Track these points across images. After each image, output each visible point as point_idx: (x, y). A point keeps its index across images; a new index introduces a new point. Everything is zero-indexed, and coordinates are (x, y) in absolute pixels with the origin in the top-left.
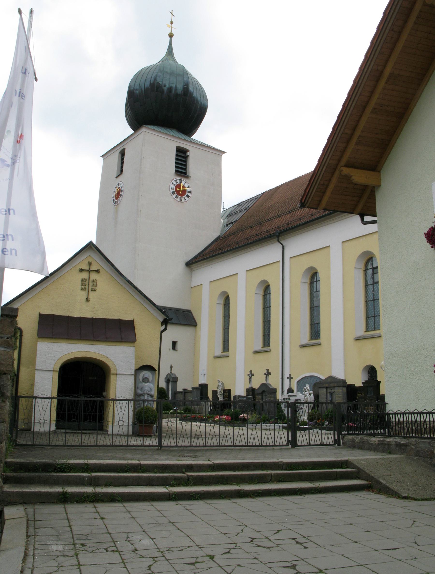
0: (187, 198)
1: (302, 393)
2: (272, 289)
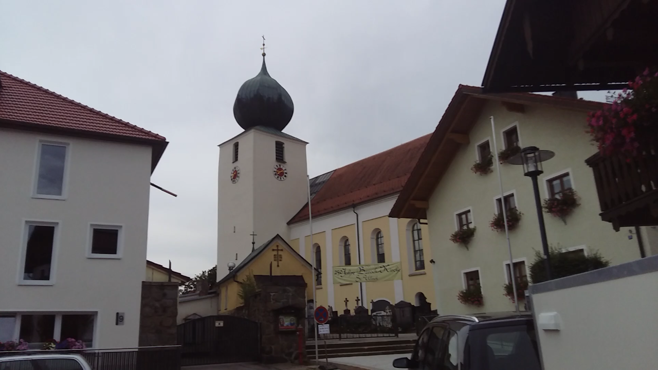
0: (285, 178)
1: (385, 312)
2: (350, 242)
